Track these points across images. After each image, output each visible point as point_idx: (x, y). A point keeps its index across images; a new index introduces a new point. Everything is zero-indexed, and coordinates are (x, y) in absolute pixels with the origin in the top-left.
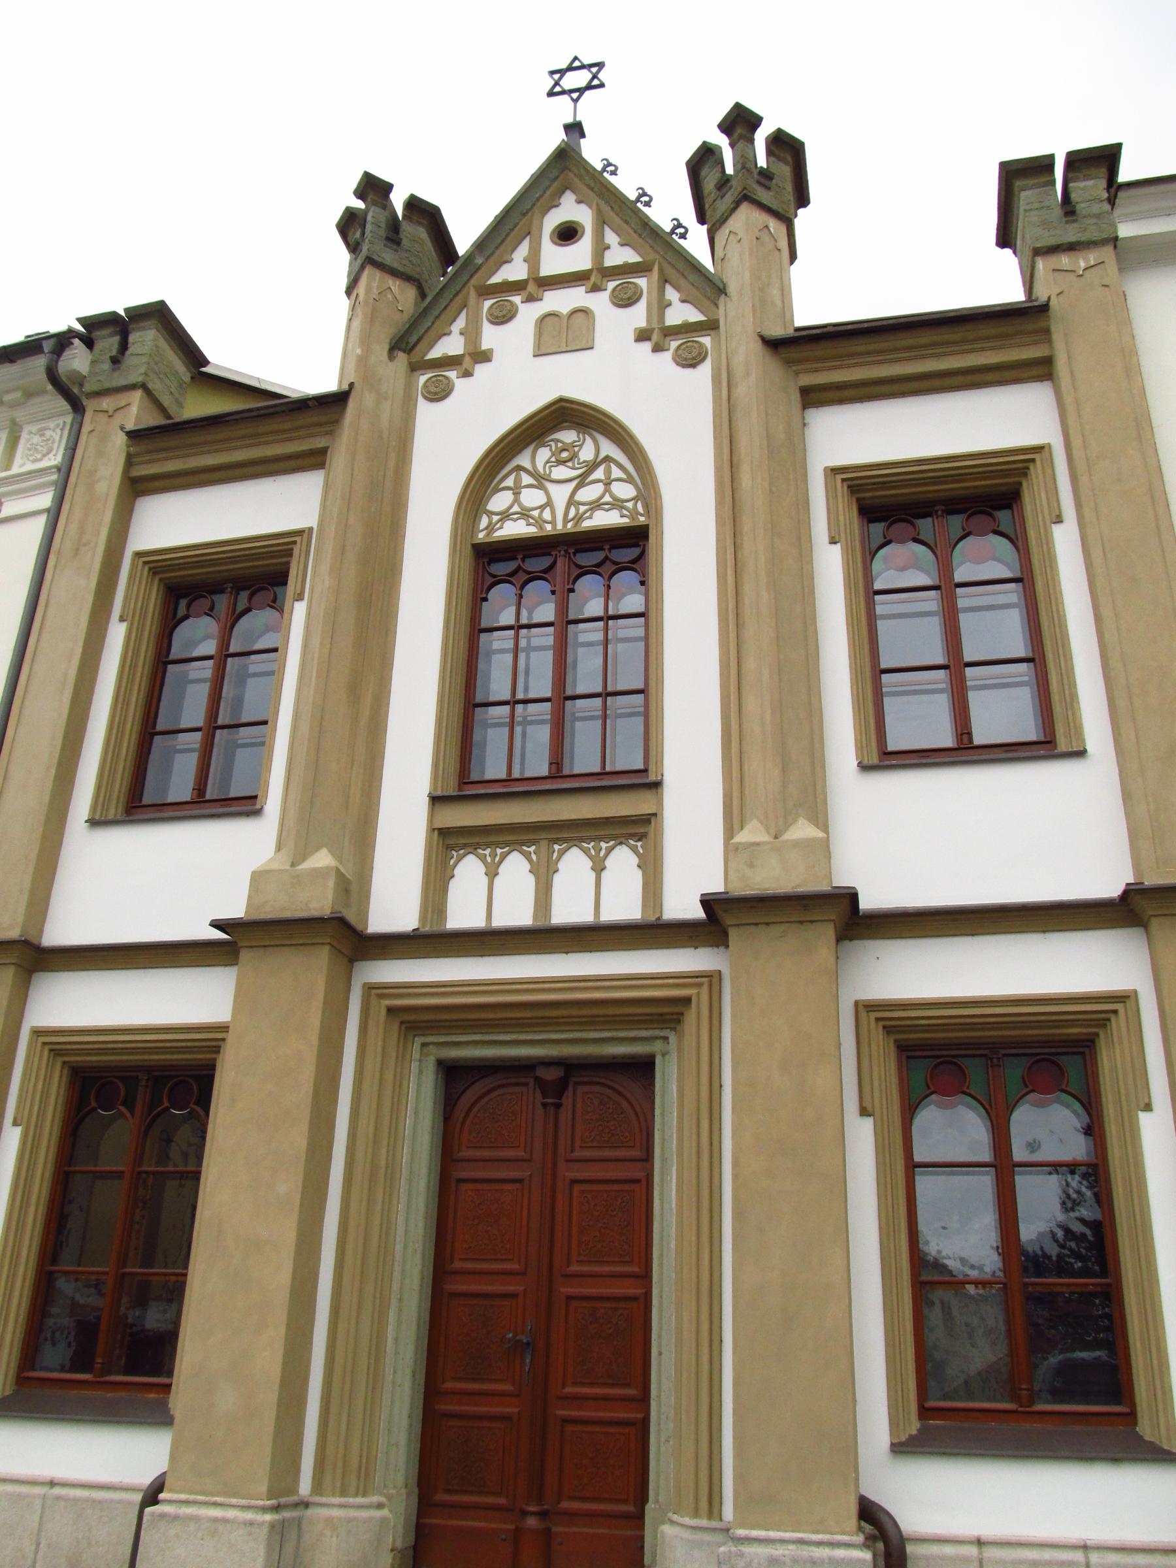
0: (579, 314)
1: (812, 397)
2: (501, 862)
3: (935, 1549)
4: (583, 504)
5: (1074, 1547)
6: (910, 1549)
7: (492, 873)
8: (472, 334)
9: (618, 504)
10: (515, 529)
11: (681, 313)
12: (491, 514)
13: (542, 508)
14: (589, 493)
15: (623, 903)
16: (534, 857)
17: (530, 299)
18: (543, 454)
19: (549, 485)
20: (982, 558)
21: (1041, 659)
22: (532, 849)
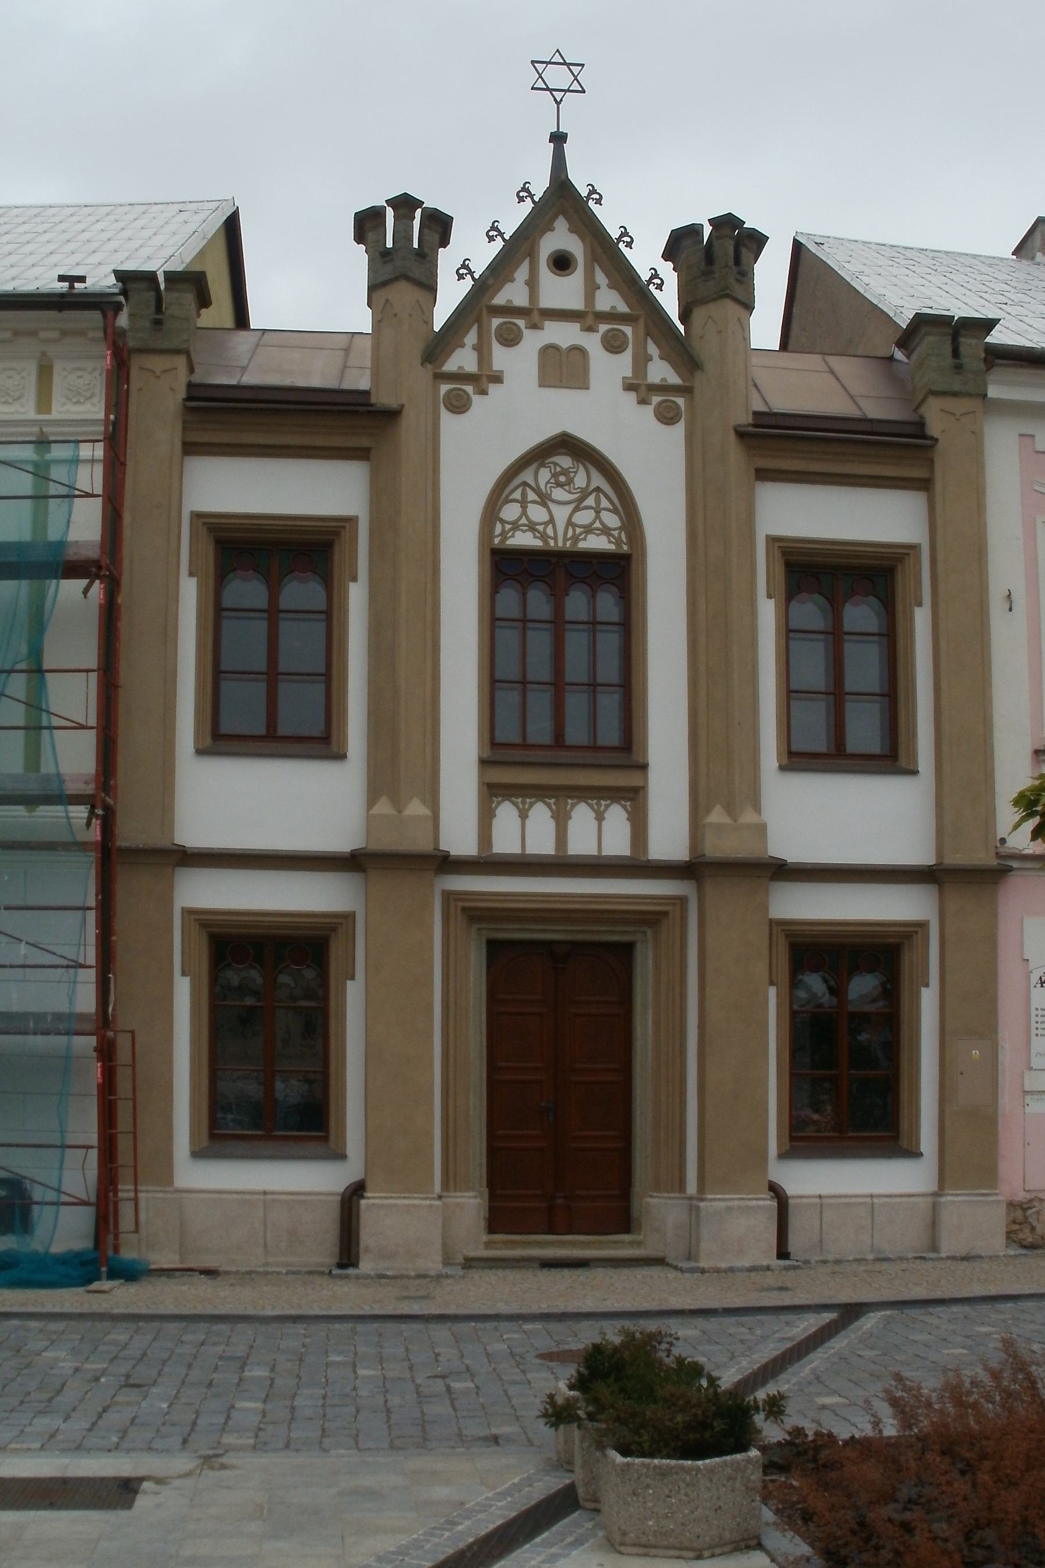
0: (577, 352)
1: (763, 475)
2: (497, 807)
3: (798, 1201)
4: (579, 526)
5: (867, 1196)
6: (791, 1201)
7: (524, 816)
8: (482, 351)
9: (606, 531)
10: (523, 540)
11: (660, 371)
12: (503, 522)
13: (546, 524)
14: (584, 517)
15: (617, 841)
16: (554, 807)
17: (534, 326)
18: (545, 475)
19: (551, 505)
20: (861, 615)
21: (893, 696)
22: (552, 801)
